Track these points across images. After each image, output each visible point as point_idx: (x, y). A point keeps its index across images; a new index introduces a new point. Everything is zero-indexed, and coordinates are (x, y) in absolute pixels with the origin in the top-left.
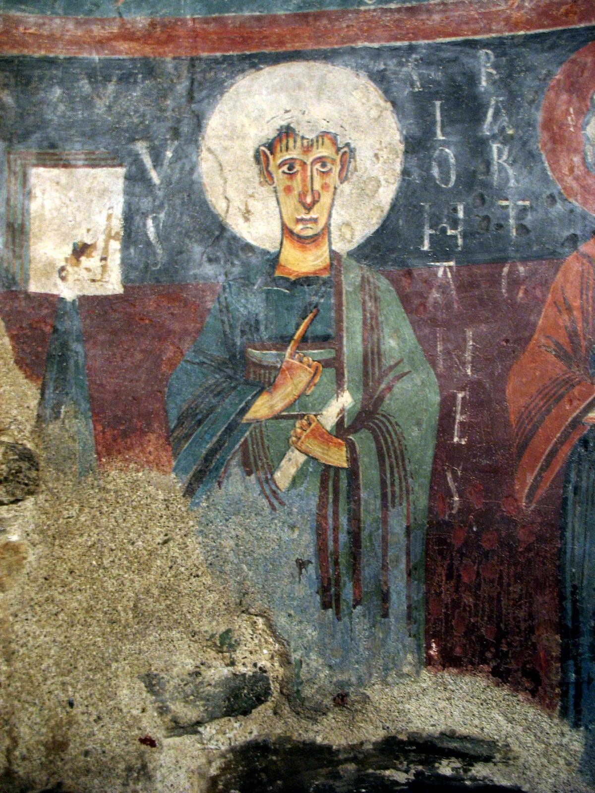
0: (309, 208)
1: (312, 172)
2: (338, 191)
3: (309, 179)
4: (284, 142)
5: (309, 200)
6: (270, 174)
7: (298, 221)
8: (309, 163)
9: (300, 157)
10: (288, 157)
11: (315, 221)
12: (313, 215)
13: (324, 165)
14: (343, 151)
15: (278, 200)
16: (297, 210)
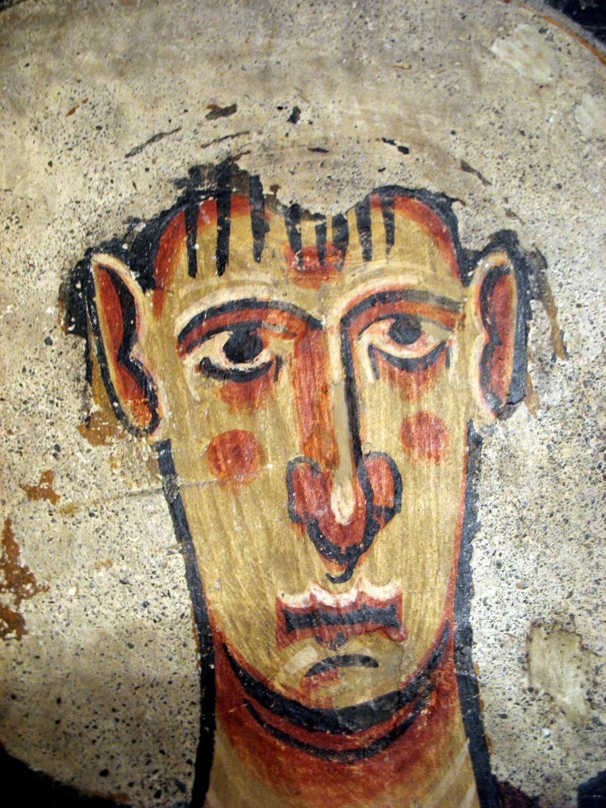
0: (346, 551)
1: (348, 360)
2: (490, 453)
3: (336, 398)
4: (209, 231)
5: (343, 505)
6: (139, 380)
7: (295, 624)
8: (331, 320)
9: (290, 295)
10: (225, 297)
11: (386, 620)
12: (373, 585)
13: (406, 330)
14: (486, 264)
15: (177, 510)
16: (286, 564)
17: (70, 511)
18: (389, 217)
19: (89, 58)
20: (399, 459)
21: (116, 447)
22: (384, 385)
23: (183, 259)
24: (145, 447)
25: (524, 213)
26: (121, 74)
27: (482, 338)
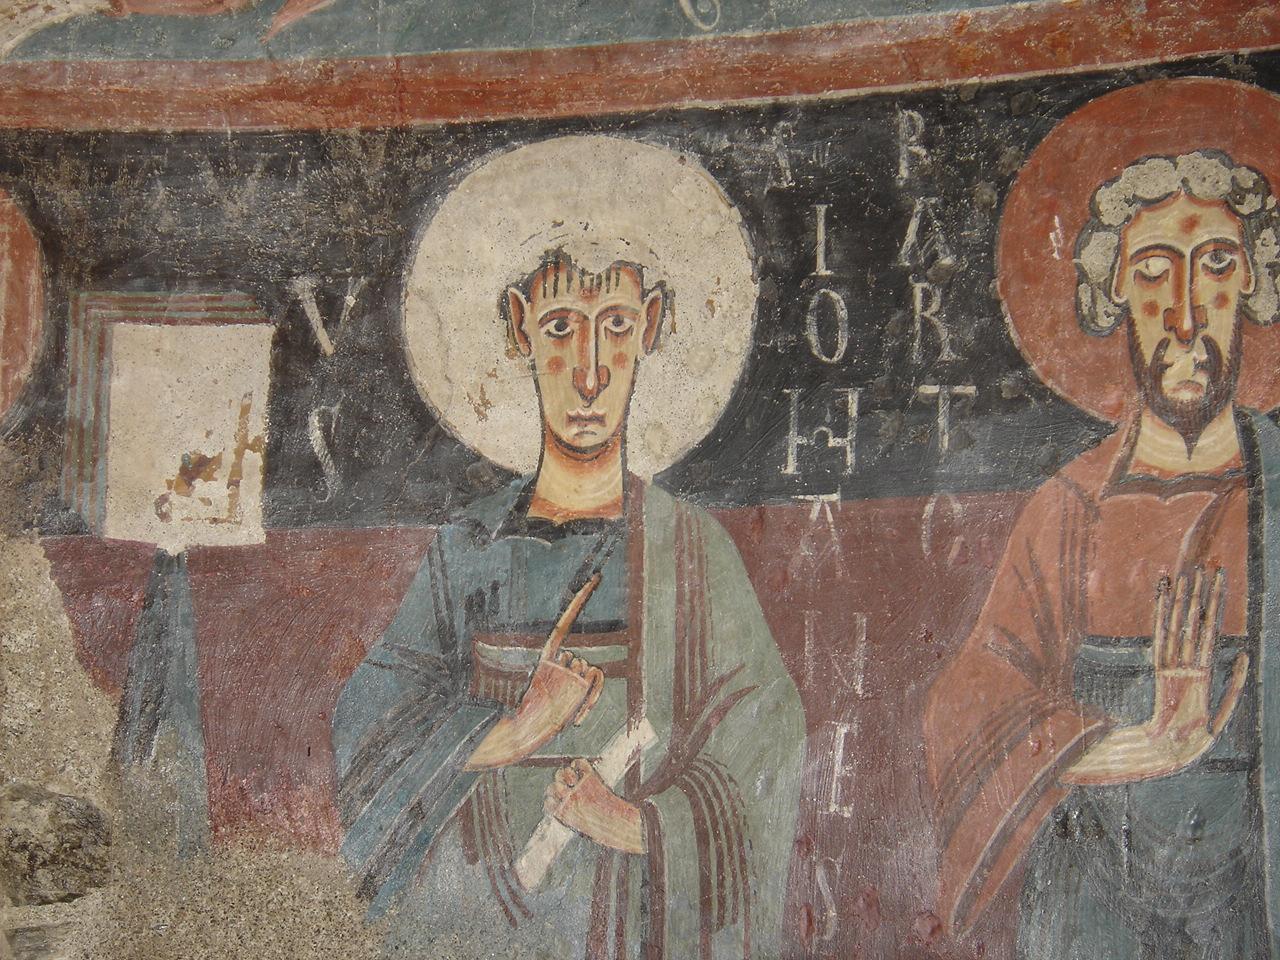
0: (589, 398)
2: (642, 366)
4: (551, 279)
6: (525, 337)
8: (592, 317)
9: (579, 306)
10: (556, 307)
11: (600, 420)
12: (597, 409)
13: (618, 322)
14: (651, 295)
17: (502, 381)
18: (618, 274)
19: (506, 198)
20: (611, 367)
21: (517, 361)
22: (609, 341)
23: (541, 291)
24: (527, 361)
25: (671, 273)
26: (518, 206)
27: (645, 325)
